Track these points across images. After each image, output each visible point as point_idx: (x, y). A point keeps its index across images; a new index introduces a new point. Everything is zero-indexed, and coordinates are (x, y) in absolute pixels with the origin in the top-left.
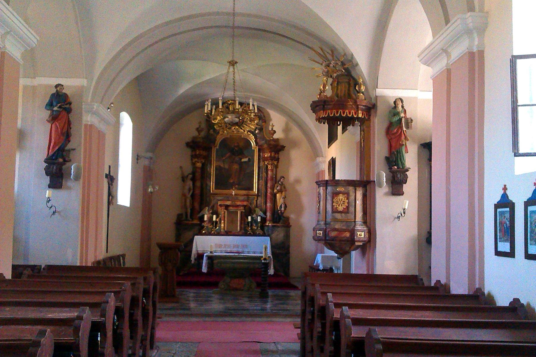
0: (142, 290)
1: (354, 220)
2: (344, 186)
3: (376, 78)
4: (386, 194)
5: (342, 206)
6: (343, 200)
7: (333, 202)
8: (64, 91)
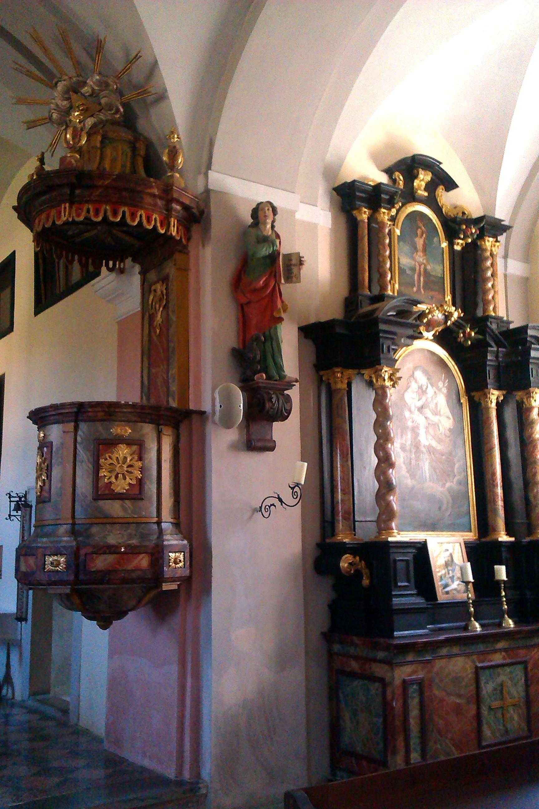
0: (447, 595)
1: (156, 519)
2: (129, 421)
3: (207, 143)
4: (234, 447)
5: (125, 478)
6: (129, 459)
7: (97, 467)
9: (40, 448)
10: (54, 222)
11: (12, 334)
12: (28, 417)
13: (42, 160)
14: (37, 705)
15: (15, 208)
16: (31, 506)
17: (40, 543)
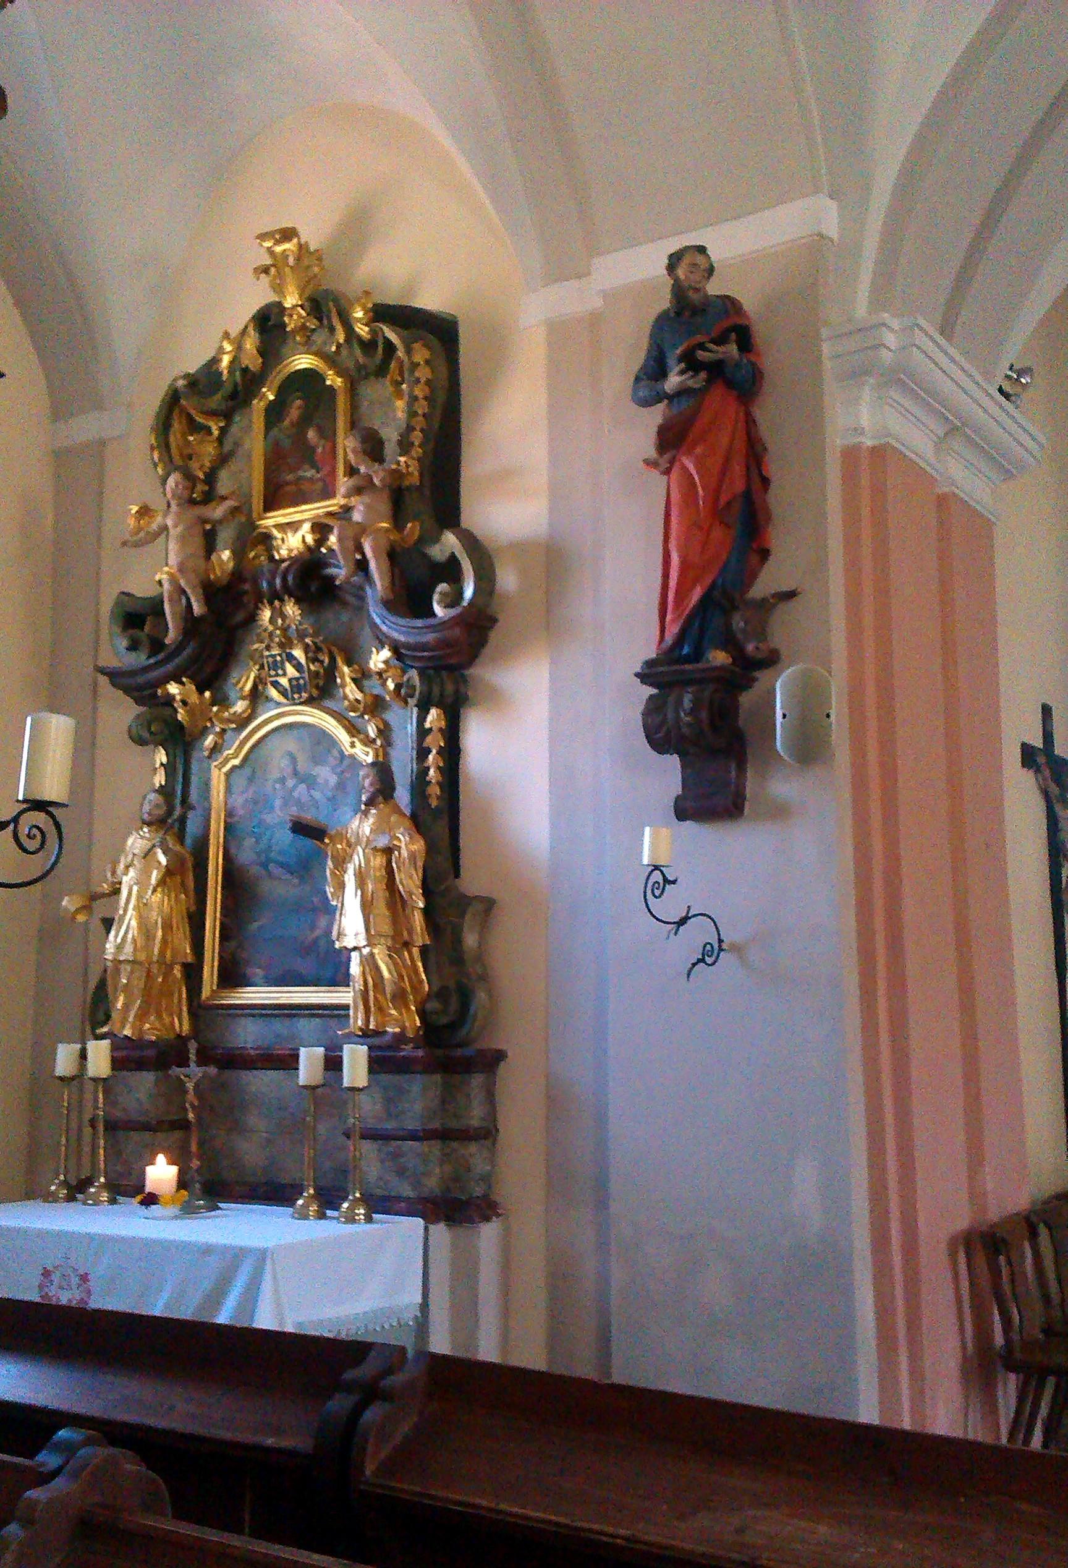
8: (714, 288)
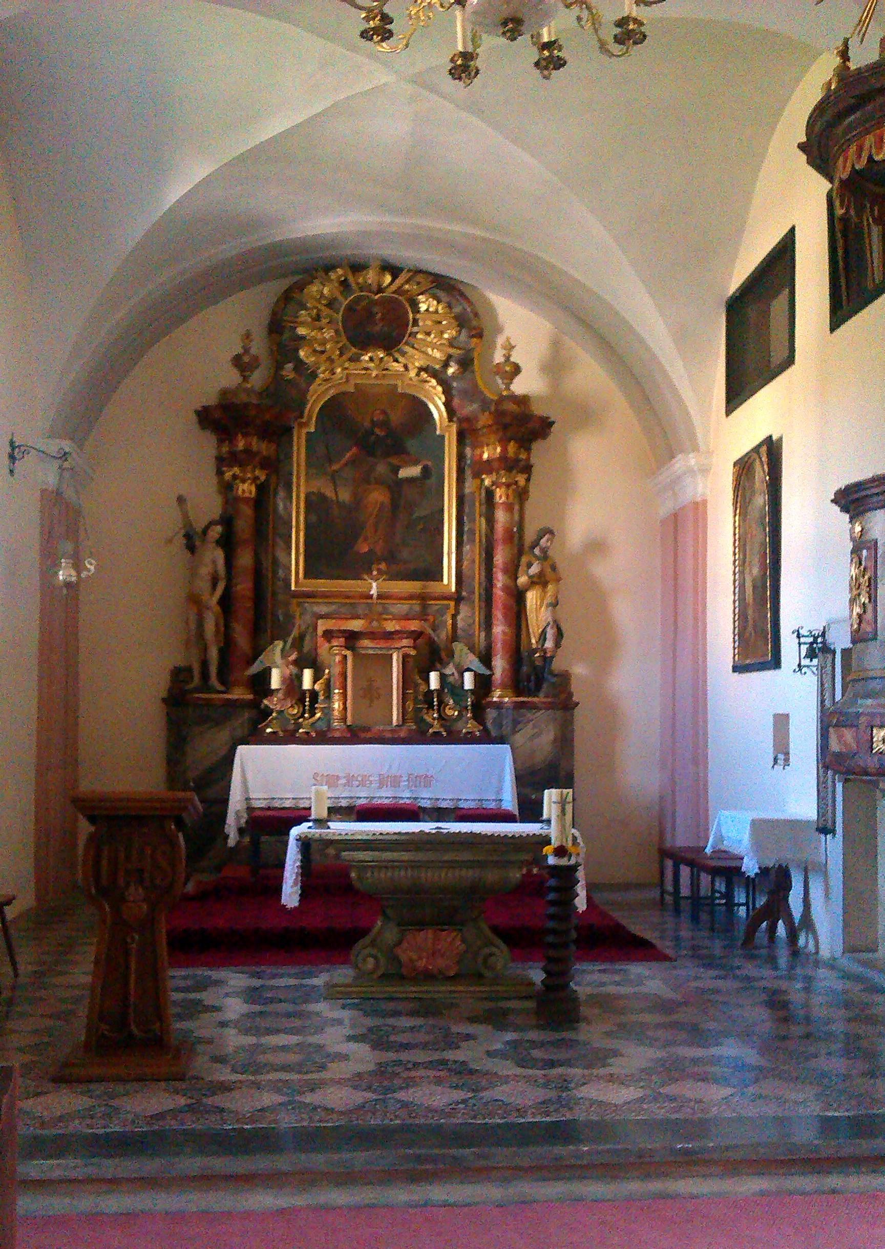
9: (856, 551)
10: (870, 158)
11: (793, 369)
12: (832, 501)
13: (844, 55)
14: (857, 969)
15: (802, 147)
16: (834, 652)
17: (861, 706)
